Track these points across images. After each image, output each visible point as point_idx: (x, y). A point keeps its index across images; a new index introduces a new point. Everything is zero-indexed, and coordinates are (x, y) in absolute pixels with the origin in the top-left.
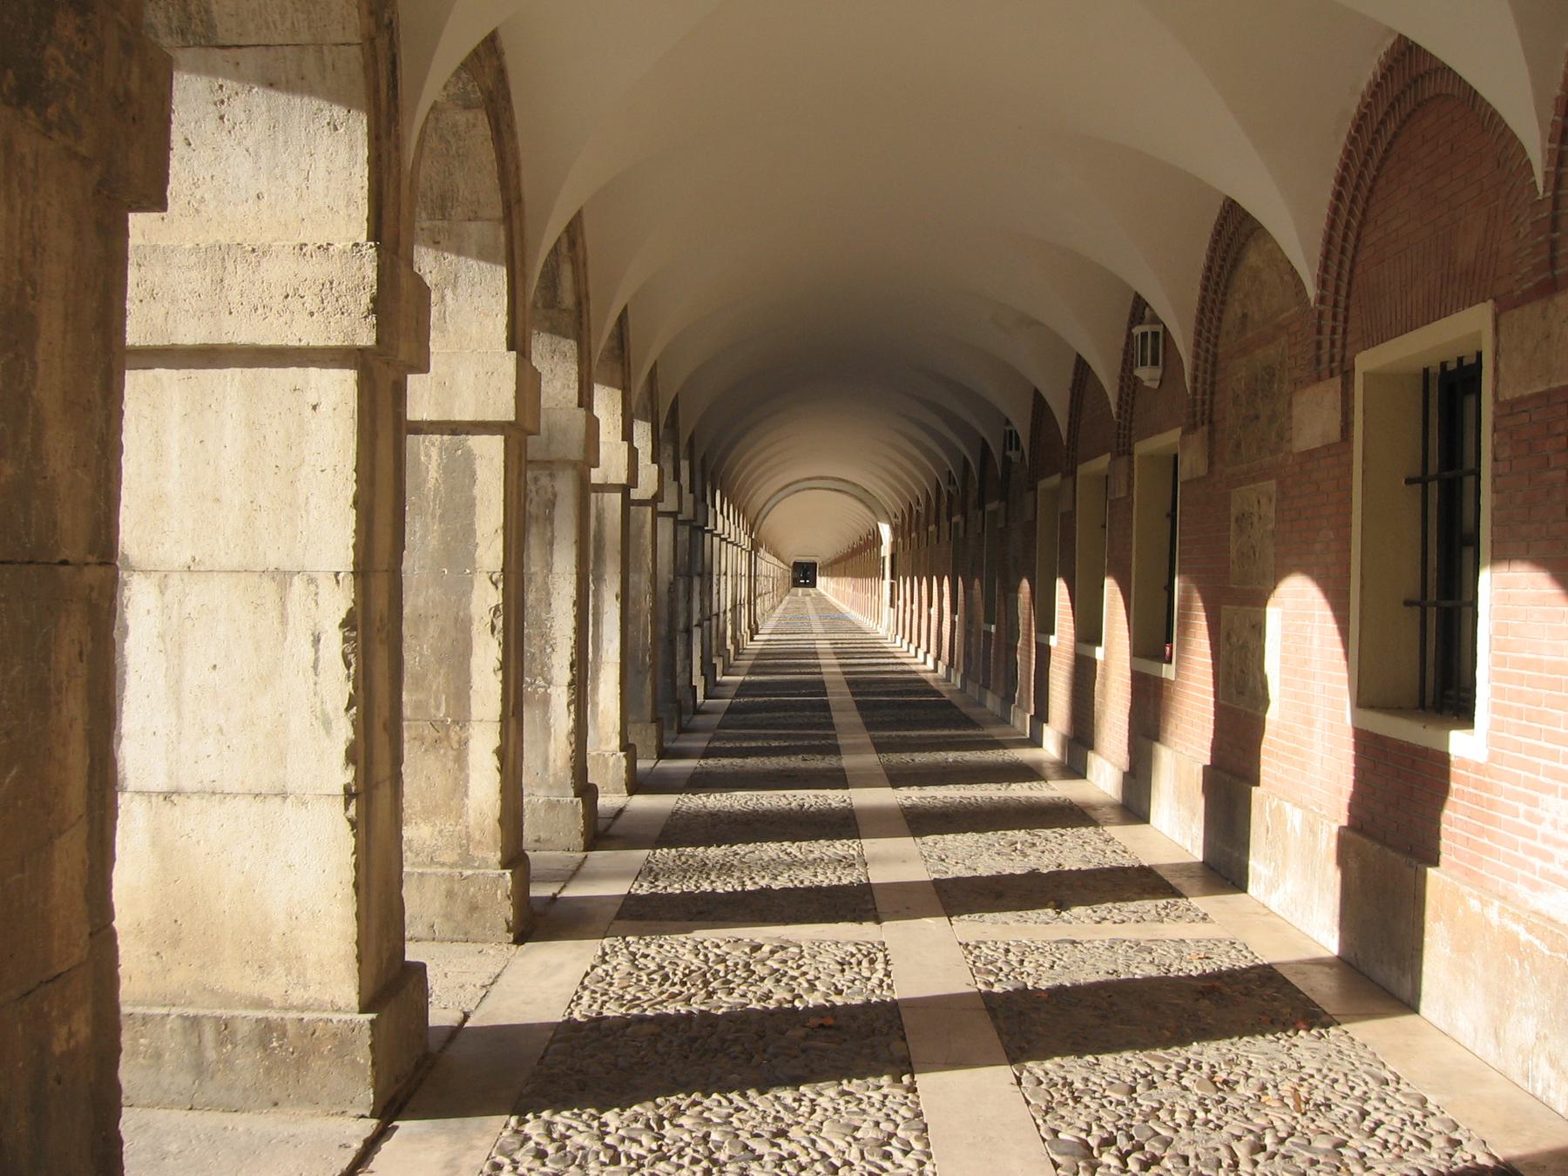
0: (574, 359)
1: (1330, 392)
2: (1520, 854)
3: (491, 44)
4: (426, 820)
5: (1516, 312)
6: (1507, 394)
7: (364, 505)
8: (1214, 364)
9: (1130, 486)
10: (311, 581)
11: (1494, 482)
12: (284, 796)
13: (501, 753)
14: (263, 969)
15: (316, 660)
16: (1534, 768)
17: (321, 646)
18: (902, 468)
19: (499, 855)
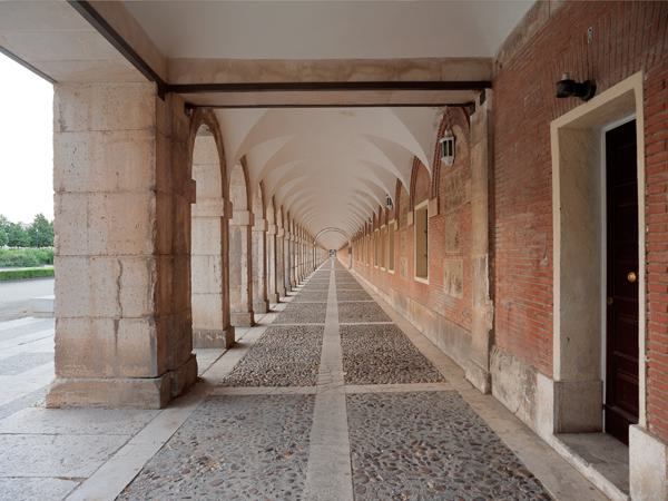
3: (244, 157)
7: (222, 243)
18: (361, 211)
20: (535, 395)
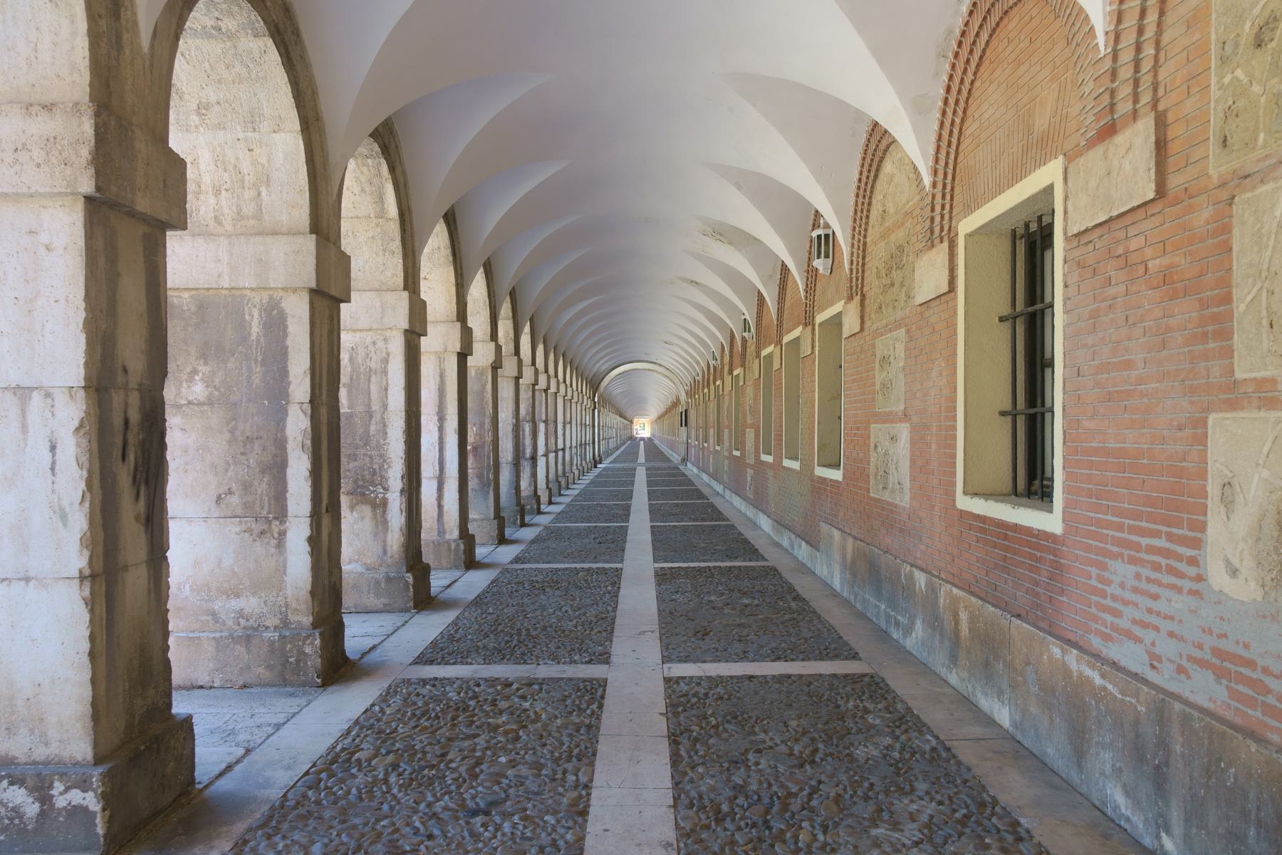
0: (400, 256)
1: (940, 254)
2: (1093, 610)
4: (254, 594)
5: (1082, 159)
6: (1074, 230)
8: (864, 251)
9: (813, 347)
10: (48, 395)
11: (1065, 305)
12: (27, 580)
13: (313, 541)
14: (10, 730)
15: (54, 463)
16: (1103, 538)
17: (58, 451)
18: (686, 352)
19: (311, 618)
20: (761, 551)
